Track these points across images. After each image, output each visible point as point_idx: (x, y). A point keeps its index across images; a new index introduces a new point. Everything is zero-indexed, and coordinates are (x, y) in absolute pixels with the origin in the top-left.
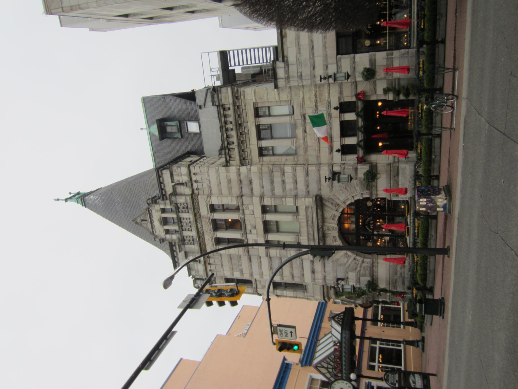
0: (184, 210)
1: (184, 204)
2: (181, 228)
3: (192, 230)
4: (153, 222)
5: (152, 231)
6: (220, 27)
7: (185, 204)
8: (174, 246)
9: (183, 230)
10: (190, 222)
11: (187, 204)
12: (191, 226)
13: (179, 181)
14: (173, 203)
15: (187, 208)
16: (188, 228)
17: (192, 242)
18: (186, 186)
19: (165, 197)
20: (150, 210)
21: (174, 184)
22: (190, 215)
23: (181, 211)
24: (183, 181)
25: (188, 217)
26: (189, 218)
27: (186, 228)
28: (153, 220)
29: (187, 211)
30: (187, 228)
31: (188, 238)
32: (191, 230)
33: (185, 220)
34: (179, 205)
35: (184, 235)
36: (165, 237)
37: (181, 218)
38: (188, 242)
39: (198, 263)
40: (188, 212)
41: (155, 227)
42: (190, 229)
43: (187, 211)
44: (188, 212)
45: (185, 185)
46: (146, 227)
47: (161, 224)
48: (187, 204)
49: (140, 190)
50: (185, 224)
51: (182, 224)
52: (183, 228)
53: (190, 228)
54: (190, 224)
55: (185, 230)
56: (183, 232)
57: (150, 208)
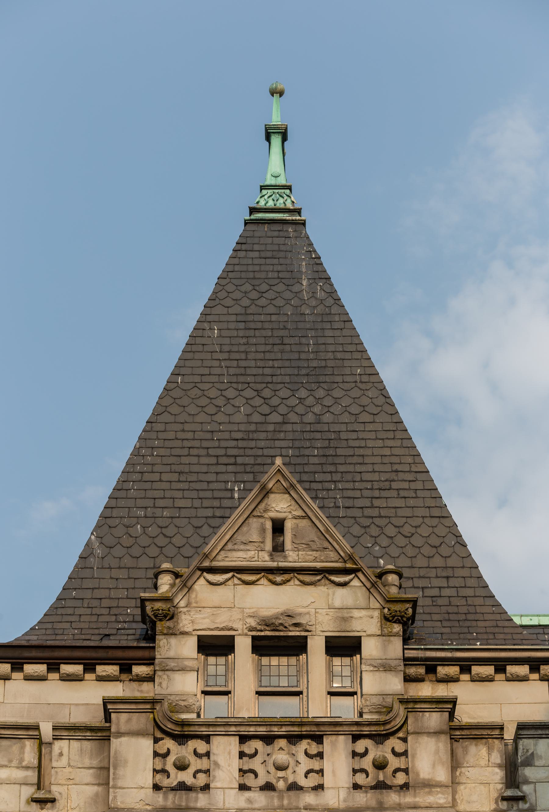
0: (367, 763)
1: (406, 771)
2: (262, 730)
3: (247, 794)
4: (274, 583)
5: (215, 564)
6: (253, 210)
7: (401, 779)
8: (126, 669)
9: (243, 739)
10: (294, 787)
11: (405, 787)
12: (268, 787)
13: (529, 762)
14: (409, 711)
15: (380, 786)
16: (261, 771)
17: (173, 781)
18: (504, 799)
19: (422, 670)
20: (347, 578)
21: (46, 730)
22: (343, 794)
23: (361, 745)
24: (527, 782)
25: (328, 780)
26: (319, 787)
27: (259, 759)
28: (284, 583)
29: (360, 779)
30: (256, 764)
31: (196, 764)
32: (243, 787)
33: (306, 764)
34: (394, 743)
35: (215, 741)
36: (184, 633)
37: (318, 739)
38: (171, 759)
39: (28, 791)
40: (356, 787)
41: (242, 589)
42: (250, 780)
43: (360, 779)
44: (356, 787)
45: (509, 793)
46: (239, 537)
47: (267, 623)
48: (405, 787)
49: (417, 541)
50: (282, 757)
51: (283, 743)
52: (257, 745)
53: (261, 781)
54: (281, 785)
55: (242, 755)
56: (235, 740)
57: (356, 583)
